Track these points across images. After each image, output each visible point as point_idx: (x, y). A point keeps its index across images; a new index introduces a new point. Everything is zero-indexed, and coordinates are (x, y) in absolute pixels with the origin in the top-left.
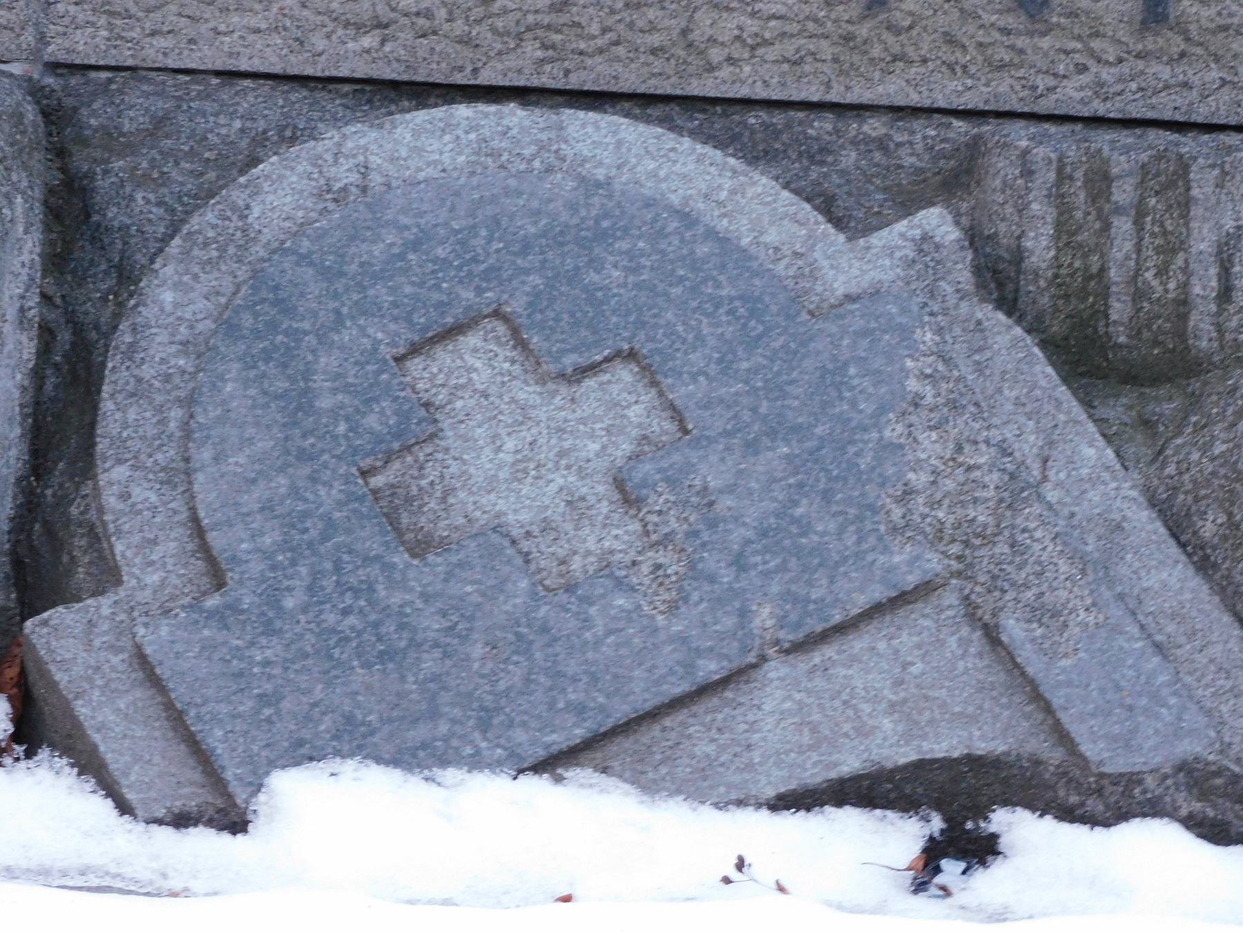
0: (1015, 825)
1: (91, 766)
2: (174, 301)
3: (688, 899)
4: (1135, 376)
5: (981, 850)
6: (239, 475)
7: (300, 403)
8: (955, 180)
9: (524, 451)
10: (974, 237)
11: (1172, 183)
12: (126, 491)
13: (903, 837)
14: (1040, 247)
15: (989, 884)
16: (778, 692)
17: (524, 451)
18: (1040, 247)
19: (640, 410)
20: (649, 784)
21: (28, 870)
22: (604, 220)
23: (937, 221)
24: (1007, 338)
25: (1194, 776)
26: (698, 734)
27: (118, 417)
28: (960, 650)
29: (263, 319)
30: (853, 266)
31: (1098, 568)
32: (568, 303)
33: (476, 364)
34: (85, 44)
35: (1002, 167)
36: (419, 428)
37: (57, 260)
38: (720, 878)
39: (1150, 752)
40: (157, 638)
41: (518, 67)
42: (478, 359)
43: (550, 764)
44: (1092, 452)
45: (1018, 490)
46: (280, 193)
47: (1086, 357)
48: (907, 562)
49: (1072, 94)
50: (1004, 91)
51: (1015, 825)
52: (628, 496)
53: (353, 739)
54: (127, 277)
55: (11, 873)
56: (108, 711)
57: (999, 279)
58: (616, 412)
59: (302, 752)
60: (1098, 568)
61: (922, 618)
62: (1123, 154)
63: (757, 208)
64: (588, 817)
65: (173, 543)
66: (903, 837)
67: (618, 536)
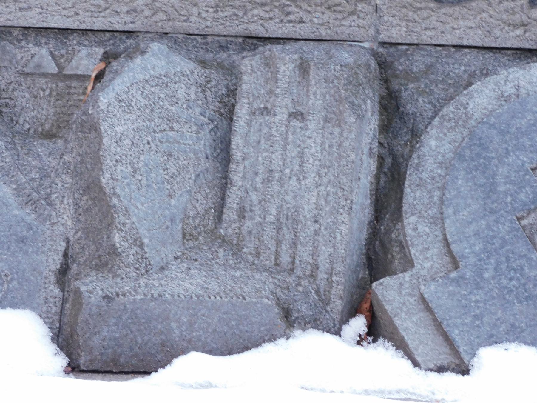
1: (401, 346)
2: (436, 144)
6: (465, 220)
7: (491, 188)
12: (416, 227)
29: (475, 152)
34: (396, 34)
37: (385, 128)
40: (429, 290)
46: (482, 98)
54: (416, 135)
59: (493, 340)
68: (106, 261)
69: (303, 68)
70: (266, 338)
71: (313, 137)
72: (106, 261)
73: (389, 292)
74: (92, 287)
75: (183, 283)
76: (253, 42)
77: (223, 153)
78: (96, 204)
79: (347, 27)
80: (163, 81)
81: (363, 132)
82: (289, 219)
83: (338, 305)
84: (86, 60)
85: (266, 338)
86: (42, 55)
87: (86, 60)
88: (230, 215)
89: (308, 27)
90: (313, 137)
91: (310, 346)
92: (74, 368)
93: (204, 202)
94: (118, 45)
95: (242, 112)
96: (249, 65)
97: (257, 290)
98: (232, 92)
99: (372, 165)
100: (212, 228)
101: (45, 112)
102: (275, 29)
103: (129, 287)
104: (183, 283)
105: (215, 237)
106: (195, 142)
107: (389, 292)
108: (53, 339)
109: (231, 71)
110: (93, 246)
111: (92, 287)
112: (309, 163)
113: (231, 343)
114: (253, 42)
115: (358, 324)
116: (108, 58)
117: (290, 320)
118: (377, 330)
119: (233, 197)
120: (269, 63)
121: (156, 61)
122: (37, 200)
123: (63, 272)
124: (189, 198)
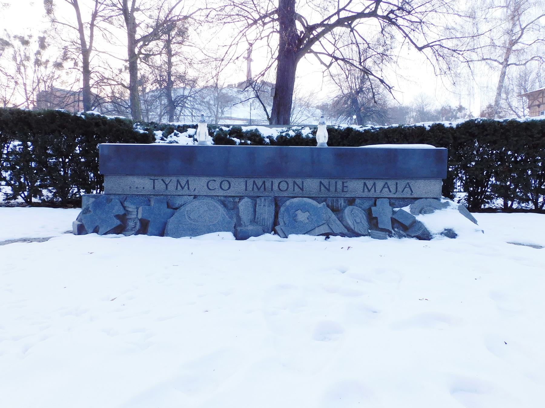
0: (331, 236)
1: (279, 235)
2: (282, 209)
3: (25, 240)
4: (336, 211)
5: (329, 238)
6: (286, 219)
7: (289, 214)
8: (325, 201)
9: (302, 216)
10: (326, 204)
11: (337, 200)
12: (280, 220)
13: (324, 237)
14: (330, 204)
15: (329, 240)
16: (317, 229)
17: (302, 216)
18: (330, 204)
19: (308, 214)
20: (310, 235)
21: (508, 58)
22: (306, 204)
23: (324, 203)
24: (328, 209)
25: (340, 233)
26: (312, 232)
27: (279, 216)
28: (327, 227)
29: (287, 210)
30: (320, 206)
31: (334, 222)
32: (304, 208)
33: (299, 212)
34: (277, 195)
35: (328, 200)
36: (296, 215)
37: (275, 207)
38: (457, 238)
39: (338, 232)
40: (282, 228)
41: (301, 195)
42: (299, 212)
43: (304, 234)
44: (333, 215)
45: (330, 218)
46: (288, 203)
47: (333, 210)
48: (324, 222)
49: (331, 196)
50: (327, 196)
51: (331, 236)
52: (308, 219)
53: (293, 233)
54: (280, 208)
55: (77, 158)
56: (280, 232)
57: (328, 206)
58: (307, 214)
59: (290, 234)
60: (334, 222)
61: (325, 225)
62: (335, 199)
63: (314, 203)
64: (307, 237)
65: (283, 222)
66: (324, 237)
67: (307, 221)
68: (240, 225)
69: (265, 200)
70: (137, 213)
71: (266, 208)
72: (240, 225)
73: (277, 228)
74: (239, 229)
75: (250, 228)
76: (258, 197)
77: (255, 211)
78: (239, 218)
79: (270, 194)
80: (247, 202)
81: (273, 208)
82: (264, 219)
83: (270, 230)
84: (237, 200)
85: (137, 213)
86: (231, 199)
87: (237, 200)
88: (256, 219)
89: (184, 88)
90: (266, 208)
91: (267, 235)
92: (237, 239)
93: (253, 217)
94: (241, 198)
95: (257, 205)
96: (258, 199)
97: (260, 228)
98: (256, 203)
99: (274, 212)
100: (254, 221)
101: (232, 206)
102: (261, 195)
103: (243, 228)
104: (250, 228)
105: (254, 222)
106: (251, 209)
107: (277, 228)
108: (240, 236)
109: (256, 201)
110: (239, 223)
111: (239, 229)
112: (266, 212)
113: (257, 235)
114: (258, 197)
115: (273, 232)
116: (240, 199)
117: (264, 232)
118: (276, 233)
119: (256, 216)
120: (261, 199)
121: (246, 199)
122: (231, 218)
123: (235, 227)
124: (250, 217)
